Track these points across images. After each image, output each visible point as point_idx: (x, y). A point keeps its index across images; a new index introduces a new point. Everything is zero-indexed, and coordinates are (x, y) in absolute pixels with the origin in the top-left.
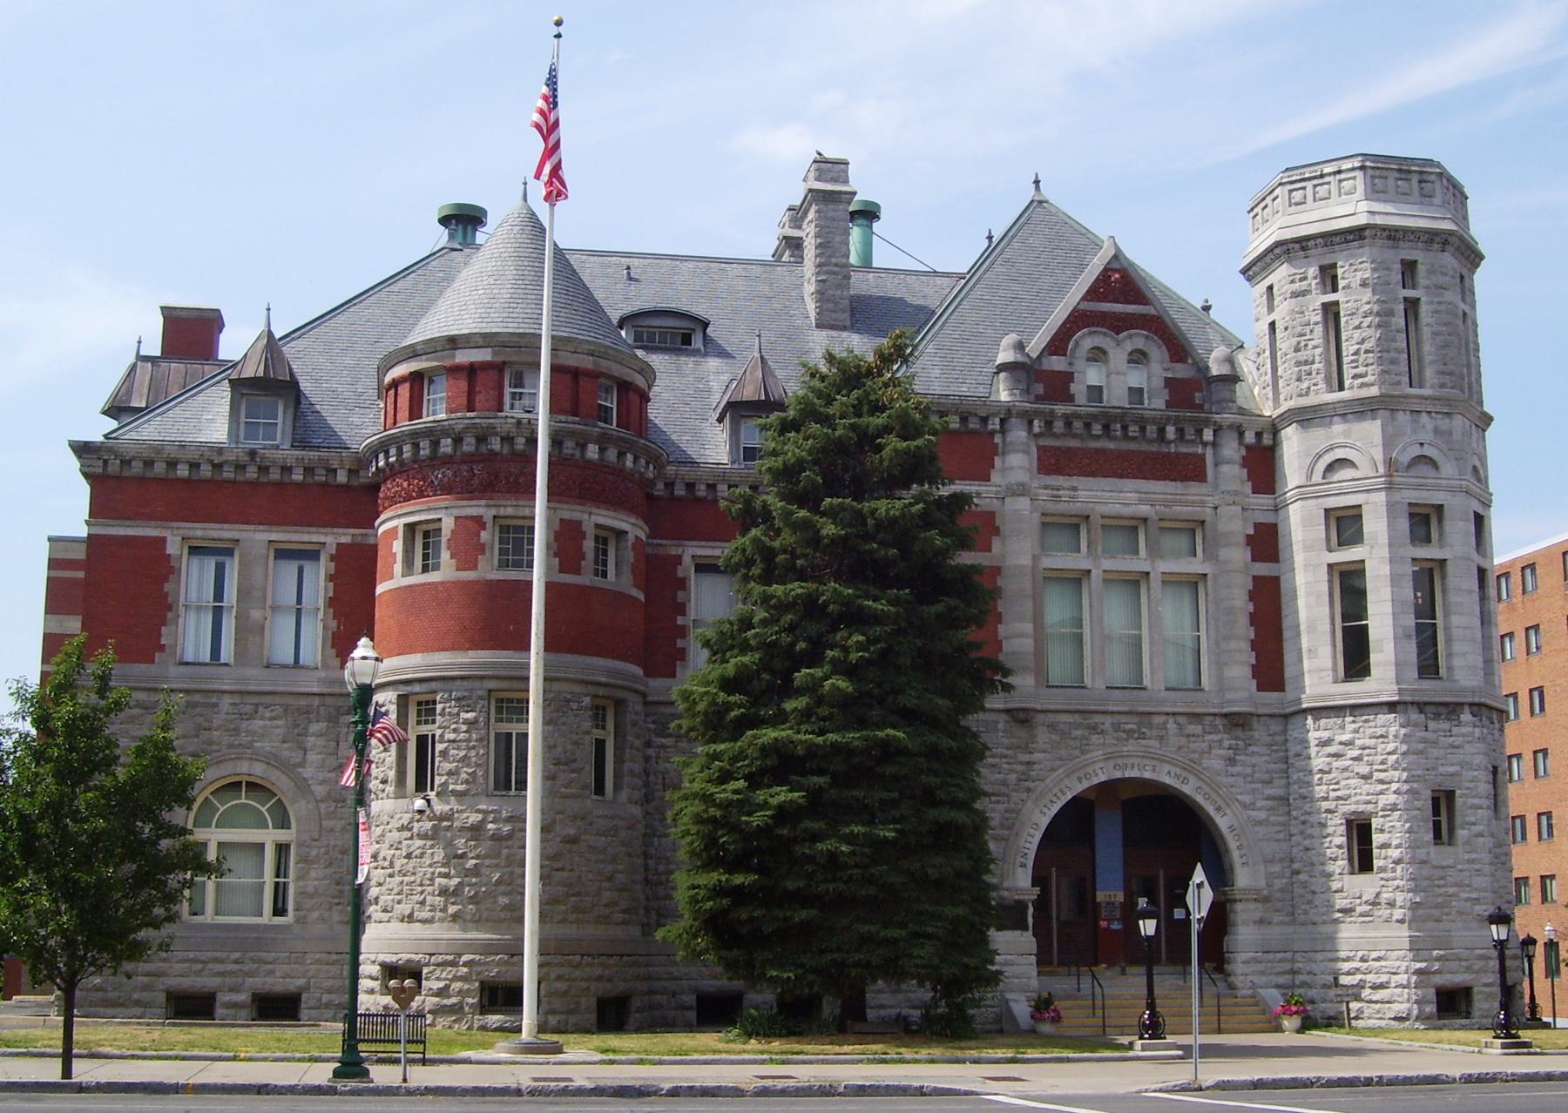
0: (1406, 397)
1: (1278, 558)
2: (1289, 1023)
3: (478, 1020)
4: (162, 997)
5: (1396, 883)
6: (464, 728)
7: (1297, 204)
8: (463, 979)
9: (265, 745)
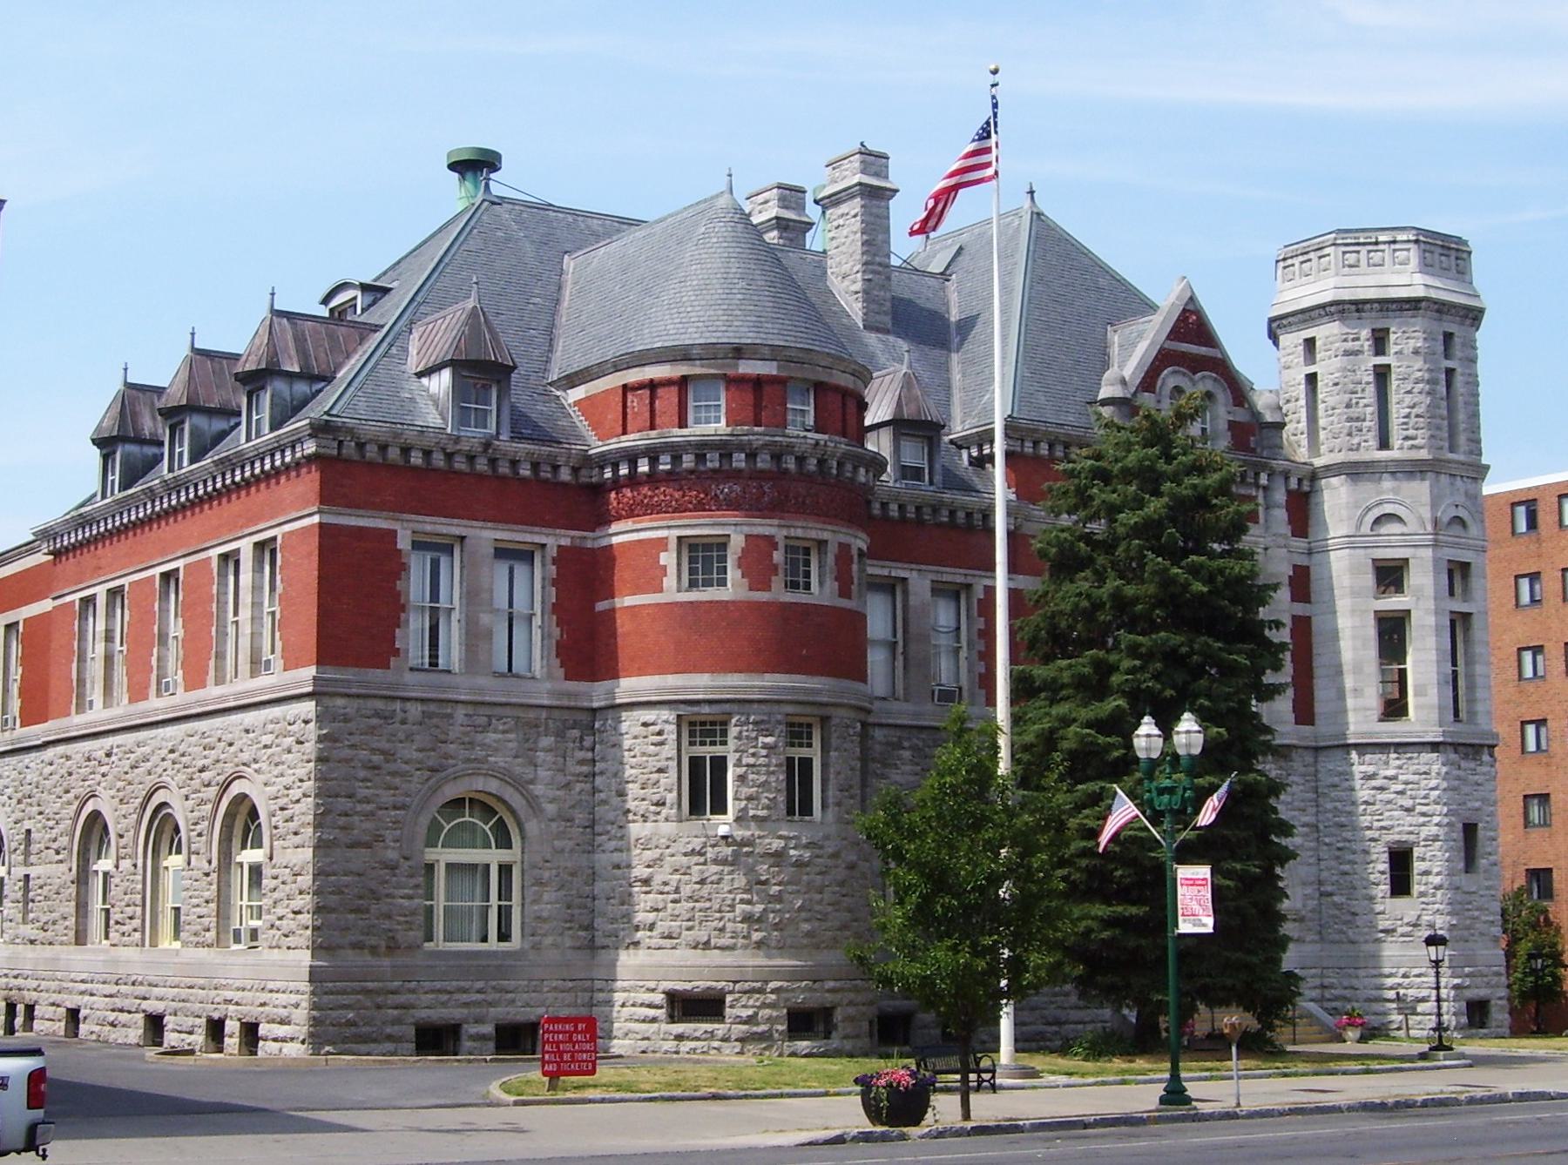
0: (1449, 461)
1: (1310, 597)
2: (1352, 1034)
3: (788, 1046)
4: (412, 1031)
5: (1436, 906)
6: (764, 752)
7: (1351, 266)
8: (772, 1006)
9: (498, 760)
